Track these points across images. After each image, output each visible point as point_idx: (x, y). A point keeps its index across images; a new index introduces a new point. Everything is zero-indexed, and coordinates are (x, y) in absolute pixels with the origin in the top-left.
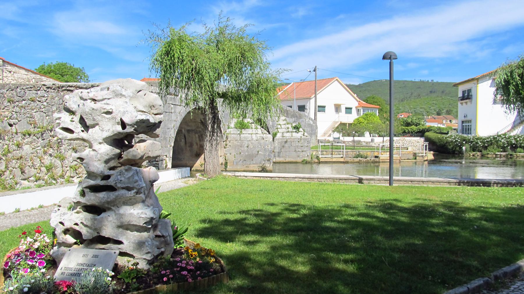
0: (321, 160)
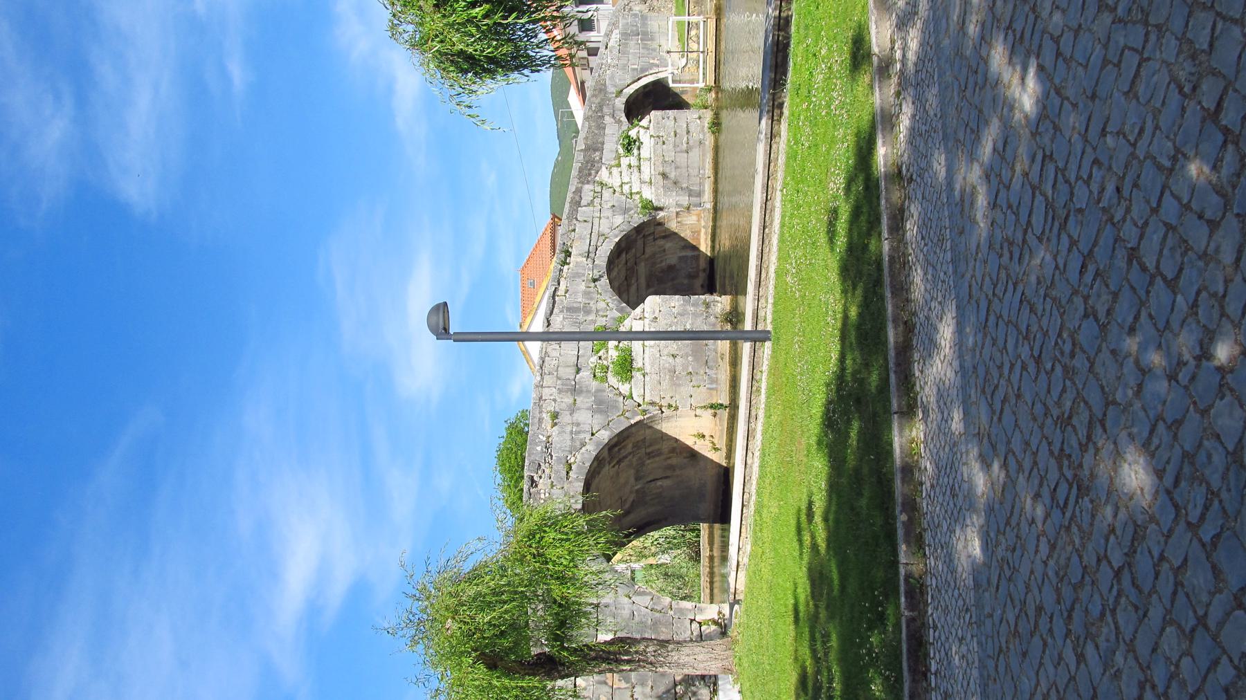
0: (711, 81)
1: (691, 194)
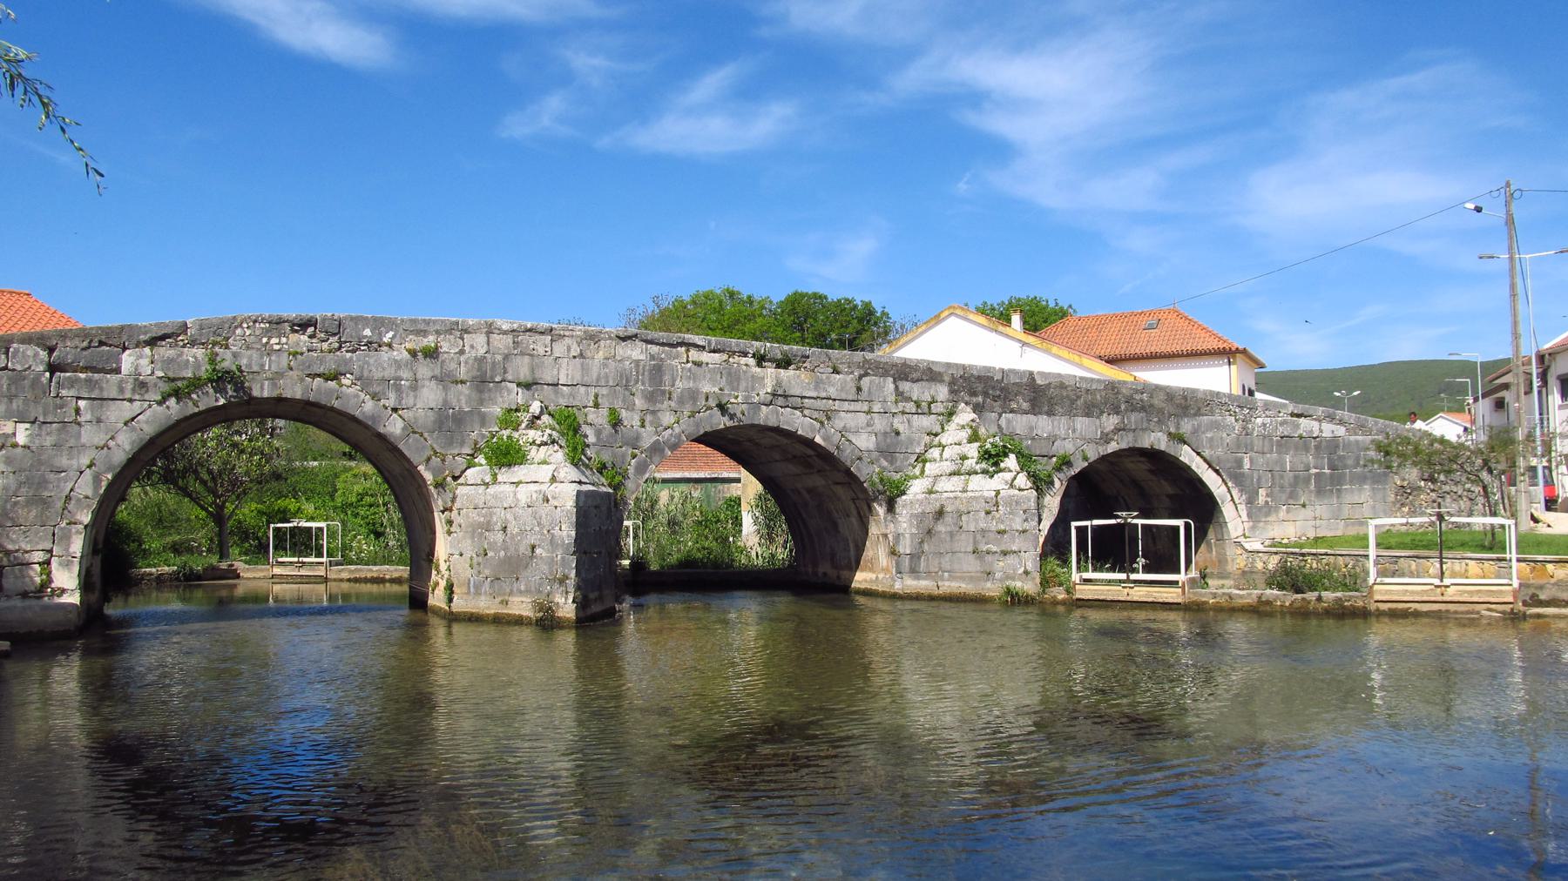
1: (915, 557)
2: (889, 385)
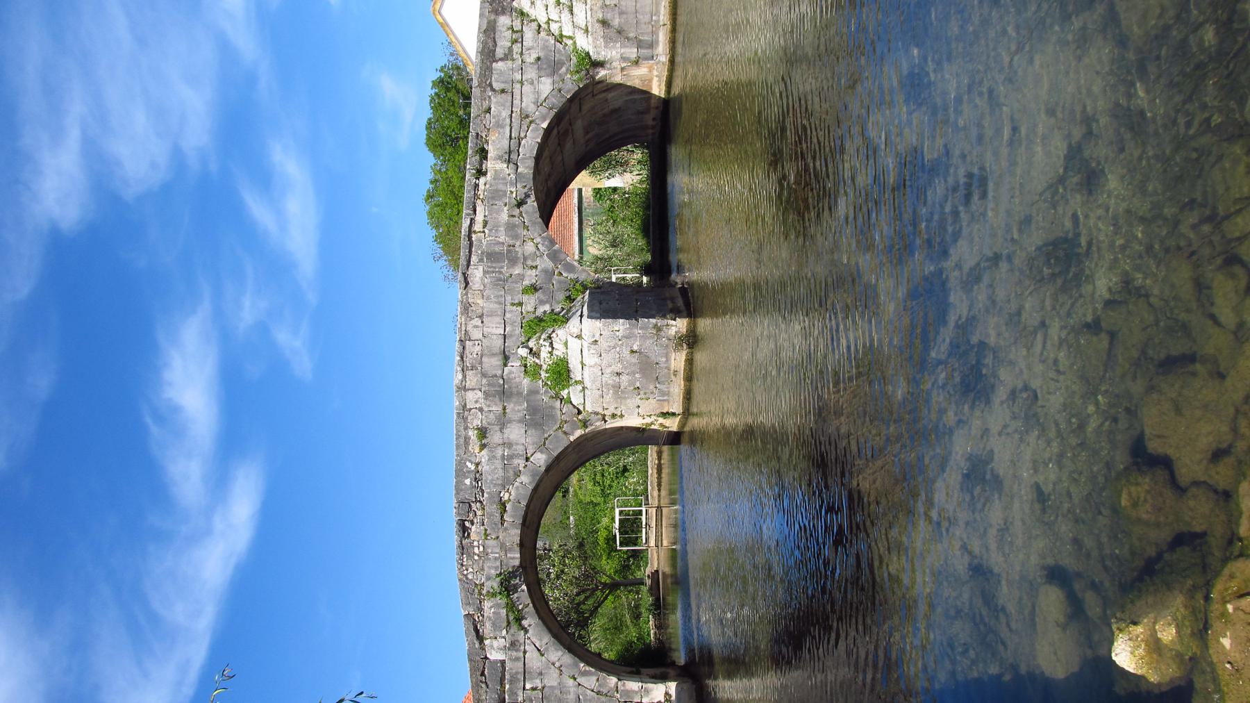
1: (640, 45)
2: (499, 66)
